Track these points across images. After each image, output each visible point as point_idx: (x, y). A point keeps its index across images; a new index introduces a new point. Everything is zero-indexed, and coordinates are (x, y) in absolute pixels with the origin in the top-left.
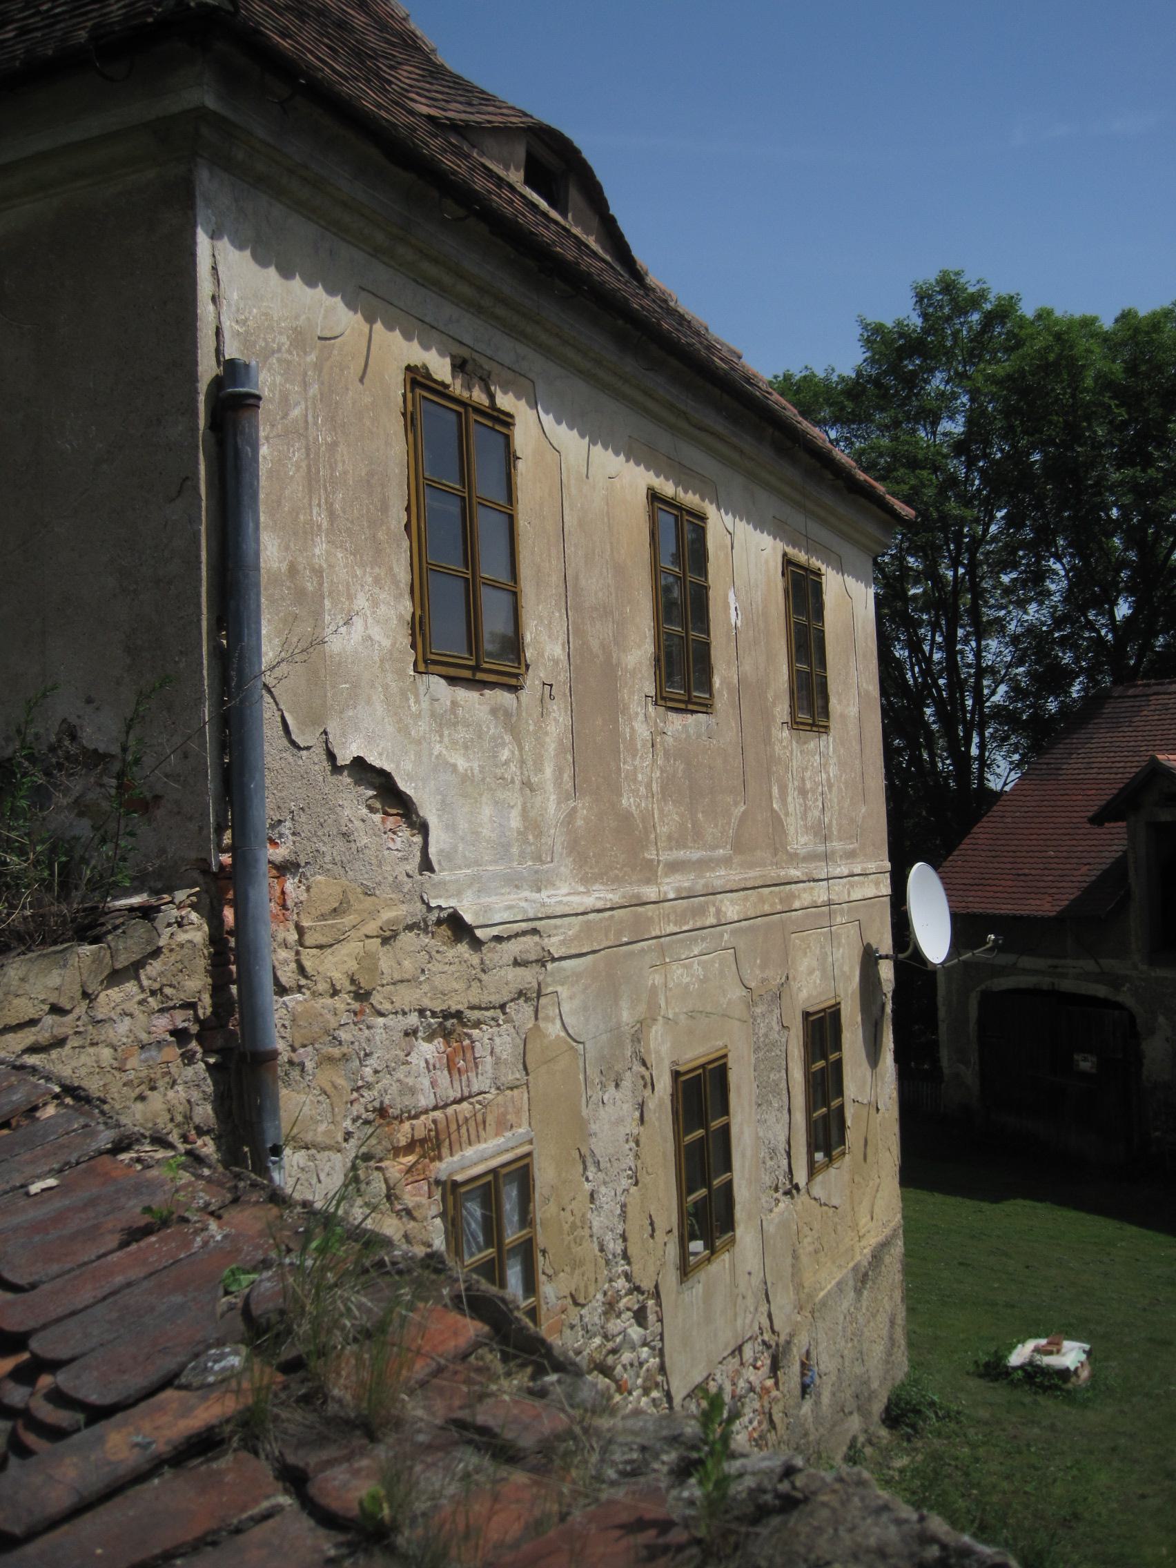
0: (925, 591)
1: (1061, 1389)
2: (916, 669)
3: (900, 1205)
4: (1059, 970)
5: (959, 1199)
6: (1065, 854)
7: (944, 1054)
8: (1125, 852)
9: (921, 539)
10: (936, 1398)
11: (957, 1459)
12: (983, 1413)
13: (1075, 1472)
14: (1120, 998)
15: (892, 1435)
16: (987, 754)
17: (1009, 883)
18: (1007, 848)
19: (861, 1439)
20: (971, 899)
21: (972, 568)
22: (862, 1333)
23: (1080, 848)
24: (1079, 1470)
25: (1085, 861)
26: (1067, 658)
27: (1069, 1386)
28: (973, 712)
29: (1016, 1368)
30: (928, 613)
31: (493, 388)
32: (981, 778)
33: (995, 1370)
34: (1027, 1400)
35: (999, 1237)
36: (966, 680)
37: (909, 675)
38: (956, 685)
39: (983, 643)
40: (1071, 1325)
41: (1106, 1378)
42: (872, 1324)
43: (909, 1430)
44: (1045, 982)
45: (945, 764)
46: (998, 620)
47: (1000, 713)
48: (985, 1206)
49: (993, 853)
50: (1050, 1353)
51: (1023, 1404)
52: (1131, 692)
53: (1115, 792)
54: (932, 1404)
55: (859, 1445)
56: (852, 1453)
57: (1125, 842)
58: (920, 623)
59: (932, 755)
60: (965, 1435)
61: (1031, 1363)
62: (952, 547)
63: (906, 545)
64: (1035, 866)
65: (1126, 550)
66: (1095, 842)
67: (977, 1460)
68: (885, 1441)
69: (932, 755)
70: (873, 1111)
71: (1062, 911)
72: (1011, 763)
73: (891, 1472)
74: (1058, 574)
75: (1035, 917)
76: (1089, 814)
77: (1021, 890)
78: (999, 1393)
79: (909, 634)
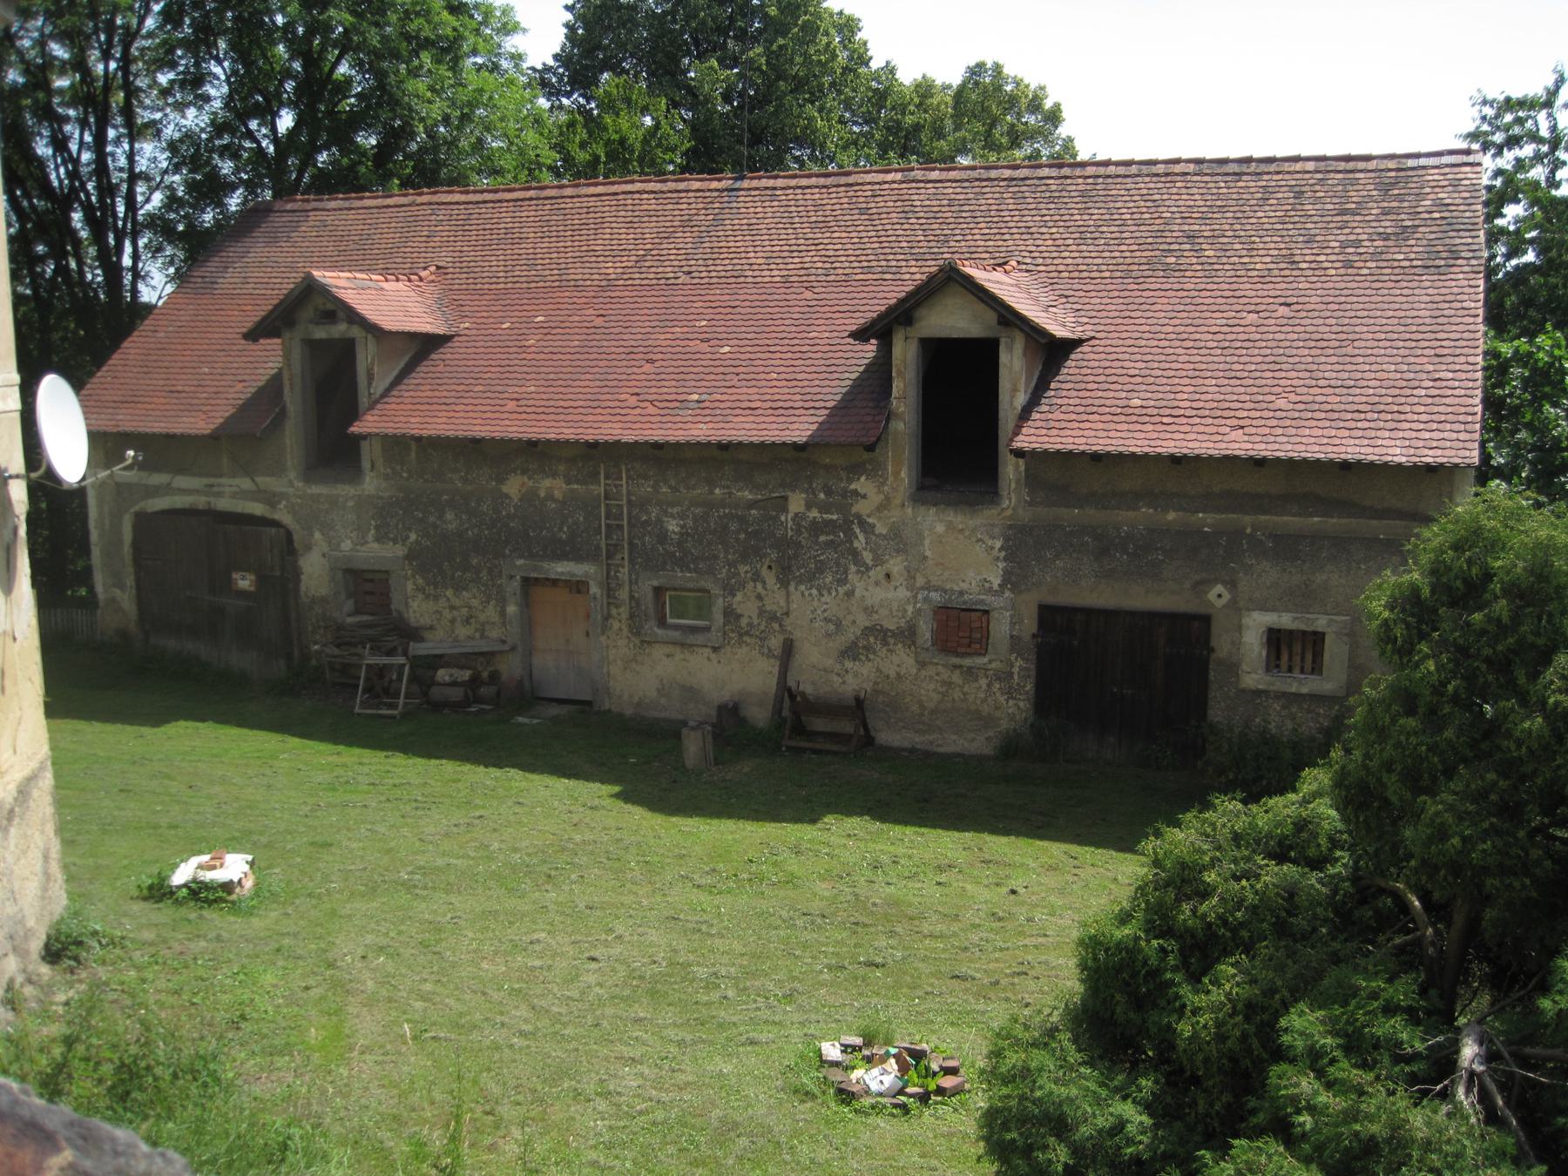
0: (72, 85)
1: (226, 901)
2: (62, 170)
3: (47, 735)
4: (215, 489)
5: (119, 726)
6: (220, 371)
7: (99, 580)
8: (280, 369)
9: (67, 21)
10: (98, 927)
11: (123, 983)
12: (148, 935)
13: (242, 977)
14: (276, 516)
15: (53, 970)
16: (140, 265)
17: (162, 400)
18: (160, 364)
19: (19, 979)
20: (121, 417)
21: (126, 61)
22: (12, 872)
23: (235, 365)
24: (246, 974)
25: (240, 378)
26: (226, 167)
27: (234, 897)
28: (125, 220)
29: (179, 887)
30: (76, 108)
31: (344, 61)
32: (135, 292)
33: (159, 892)
34: (193, 916)
35: (160, 760)
36: (118, 185)
37: (53, 176)
38: (107, 190)
39: (137, 146)
40: (234, 838)
41: (270, 885)
42: (23, 861)
43: (72, 963)
44: (201, 502)
45: (95, 275)
46: (153, 123)
47: (154, 222)
48: (145, 730)
49: (145, 369)
50: (213, 868)
51: (189, 921)
52: (289, 206)
53: (270, 307)
54: (95, 933)
55: (17, 986)
56: (9, 996)
57: (280, 359)
58: (67, 119)
59: (80, 263)
60: (130, 958)
61: (194, 880)
62: (103, 38)
63: (48, 30)
64: (189, 383)
65: (291, 59)
66: (250, 359)
67: (144, 981)
68: (47, 978)
69: (80, 263)
70: (9, 640)
71: (217, 429)
72: (167, 276)
73: (54, 1008)
74: (218, 79)
75: (189, 436)
76: (244, 330)
77: (175, 407)
78: (164, 913)
79: (53, 130)
